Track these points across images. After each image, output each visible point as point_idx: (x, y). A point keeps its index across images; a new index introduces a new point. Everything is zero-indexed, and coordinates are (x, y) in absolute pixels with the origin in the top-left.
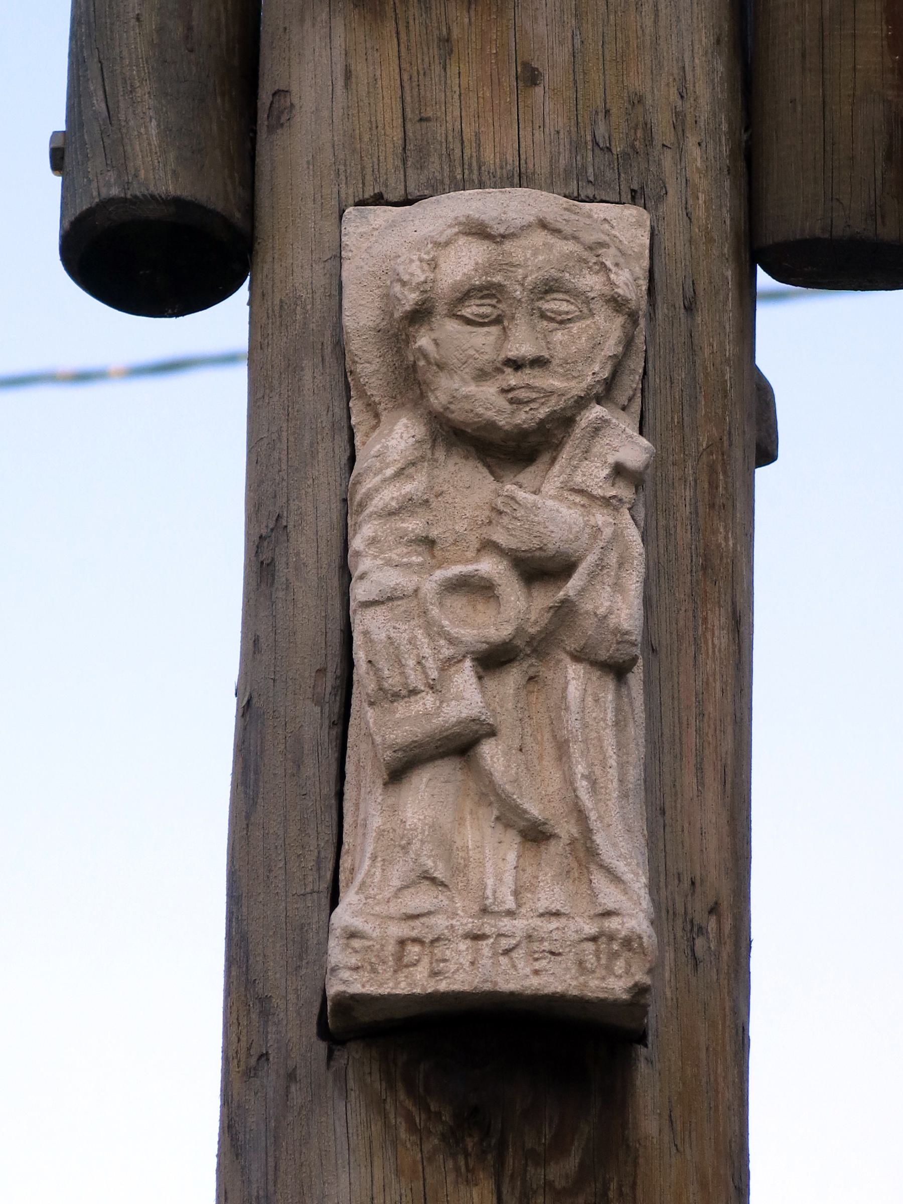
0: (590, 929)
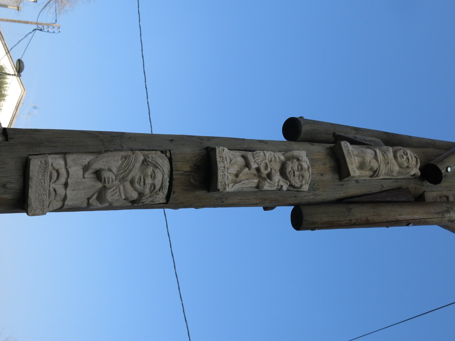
0: (226, 183)
